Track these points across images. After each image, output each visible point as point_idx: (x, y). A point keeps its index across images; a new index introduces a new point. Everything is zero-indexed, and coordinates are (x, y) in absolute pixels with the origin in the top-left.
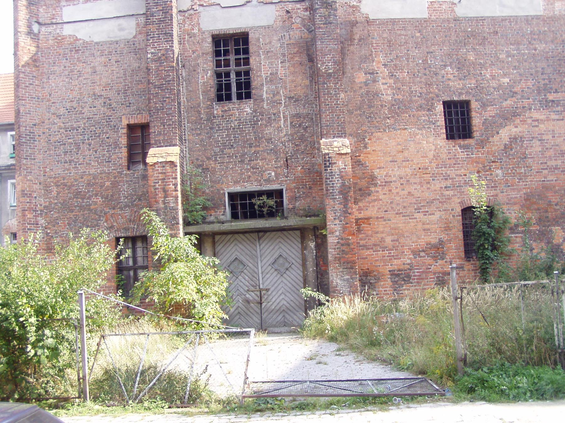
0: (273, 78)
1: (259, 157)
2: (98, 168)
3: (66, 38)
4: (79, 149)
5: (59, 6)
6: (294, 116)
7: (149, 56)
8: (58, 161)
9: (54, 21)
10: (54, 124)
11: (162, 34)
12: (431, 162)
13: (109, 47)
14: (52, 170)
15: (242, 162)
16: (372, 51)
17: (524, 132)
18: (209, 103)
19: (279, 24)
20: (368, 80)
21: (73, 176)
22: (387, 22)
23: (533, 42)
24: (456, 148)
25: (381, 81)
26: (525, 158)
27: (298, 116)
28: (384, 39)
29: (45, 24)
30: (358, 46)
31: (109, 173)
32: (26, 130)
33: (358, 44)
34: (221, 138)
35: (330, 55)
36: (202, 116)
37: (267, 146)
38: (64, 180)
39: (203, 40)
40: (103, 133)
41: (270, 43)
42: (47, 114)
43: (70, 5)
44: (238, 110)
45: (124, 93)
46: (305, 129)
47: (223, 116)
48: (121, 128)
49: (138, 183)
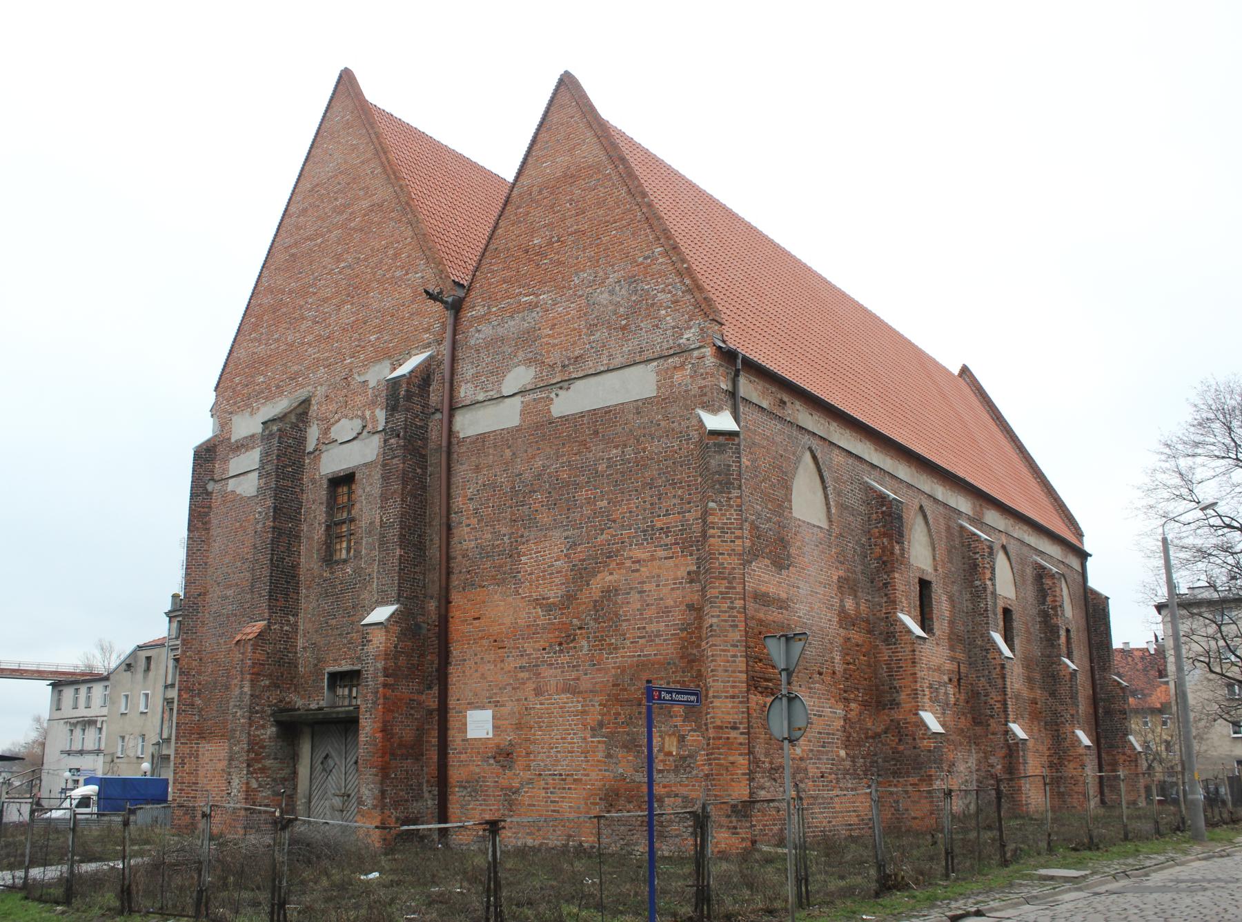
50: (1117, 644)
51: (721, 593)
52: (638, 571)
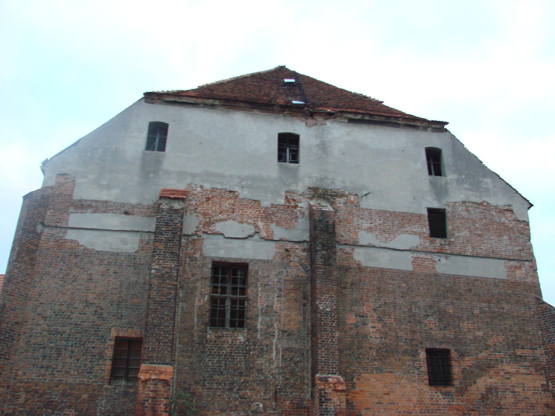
0: (268, 311)
1: (248, 387)
2: (77, 378)
3: (68, 242)
4: (59, 354)
5: (67, 212)
6: (286, 350)
7: (153, 271)
8: (34, 365)
9: (59, 225)
10: (38, 325)
11: (168, 252)
12: (415, 407)
13: (109, 258)
14: (25, 373)
15: (231, 390)
16: (362, 296)
17: (497, 383)
18: (202, 326)
19: (278, 260)
20: (358, 322)
21: (48, 383)
22: (377, 271)
23: (501, 302)
24: (436, 396)
25: (371, 324)
26: (501, 408)
27: (289, 350)
28: (374, 285)
29: (49, 226)
30: (350, 290)
31: (88, 385)
32: (7, 326)
33: (350, 288)
34: (212, 363)
35: (328, 294)
36: (195, 339)
37: (257, 377)
38: (36, 386)
39: (204, 265)
40: (90, 342)
41: (268, 276)
42: (33, 314)
43: (77, 213)
44: (231, 337)
45: (117, 304)
46: (296, 363)
47: (215, 341)
48: (110, 340)
49: (119, 399)
50: (410, 268)
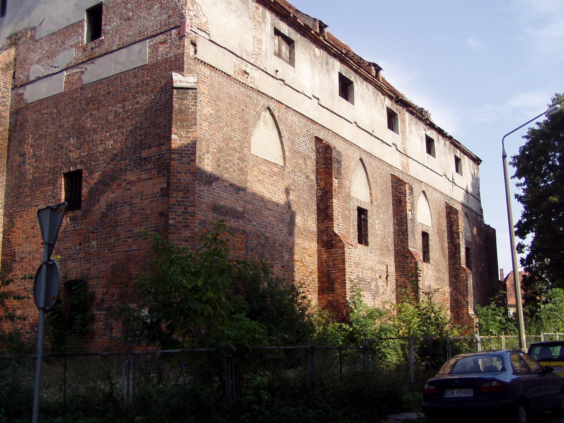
51: (177, 201)
52: (129, 189)
